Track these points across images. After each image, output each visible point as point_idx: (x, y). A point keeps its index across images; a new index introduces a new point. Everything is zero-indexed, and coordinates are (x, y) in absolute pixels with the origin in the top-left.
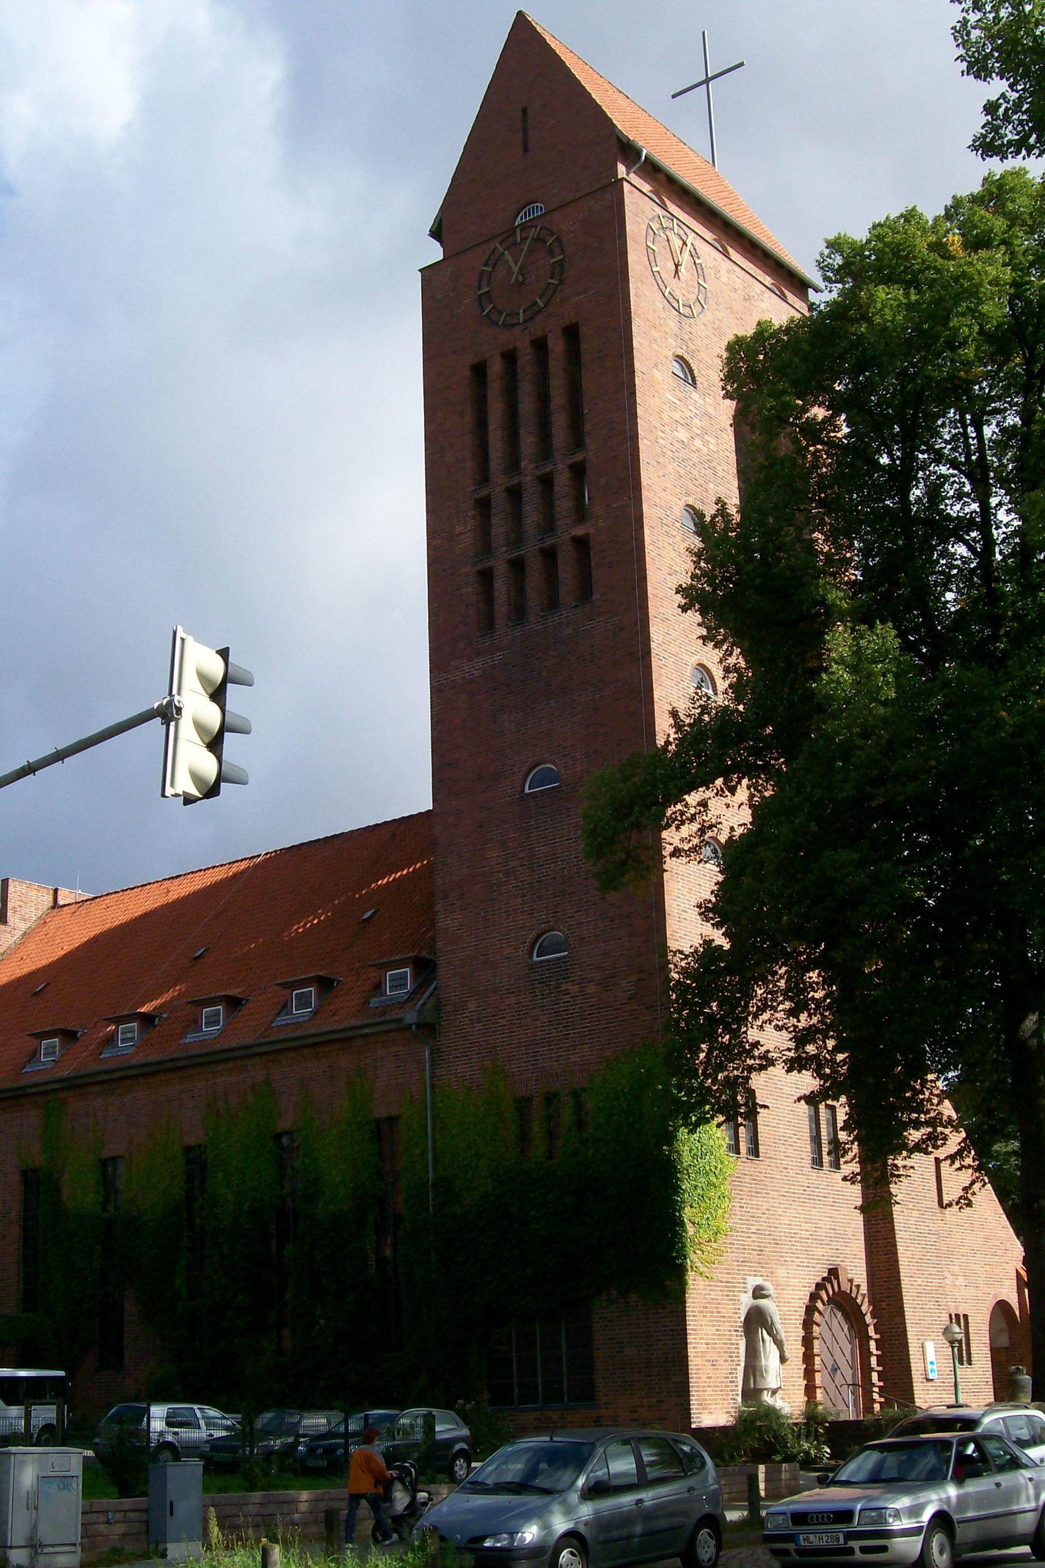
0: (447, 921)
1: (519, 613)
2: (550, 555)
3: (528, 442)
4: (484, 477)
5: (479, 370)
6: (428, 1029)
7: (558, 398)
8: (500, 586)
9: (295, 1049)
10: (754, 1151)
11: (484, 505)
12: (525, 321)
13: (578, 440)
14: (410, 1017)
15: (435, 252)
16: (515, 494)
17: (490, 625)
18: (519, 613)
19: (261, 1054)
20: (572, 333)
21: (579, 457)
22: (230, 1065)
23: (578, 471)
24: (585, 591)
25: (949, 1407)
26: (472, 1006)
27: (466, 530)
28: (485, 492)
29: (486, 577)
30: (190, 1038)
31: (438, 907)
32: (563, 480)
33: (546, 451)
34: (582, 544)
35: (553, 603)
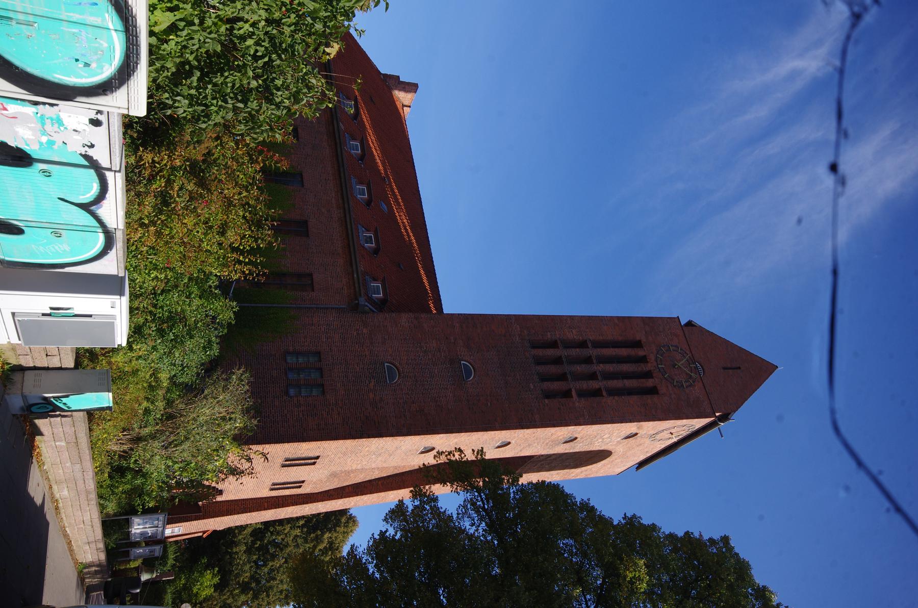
0: (405, 319)
1: (539, 361)
2: (562, 377)
3: (610, 368)
4: (597, 345)
5: (638, 344)
6: (355, 308)
7: (628, 383)
8: (551, 352)
9: (347, 235)
10: (284, 466)
11: (583, 344)
12: (657, 357)
13: (612, 392)
14: (362, 301)
15: (683, 322)
16: (588, 360)
17: (534, 346)
18: (539, 361)
19: (345, 216)
20: (653, 391)
21: (604, 393)
22: (341, 201)
23: (597, 393)
24: (549, 395)
25: (44, 315)
26: (365, 331)
27: (573, 335)
28: (590, 345)
29: (554, 345)
30: (354, 181)
31: (411, 314)
32: (594, 385)
33: (608, 376)
34: (567, 394)
35: (544, 378)
